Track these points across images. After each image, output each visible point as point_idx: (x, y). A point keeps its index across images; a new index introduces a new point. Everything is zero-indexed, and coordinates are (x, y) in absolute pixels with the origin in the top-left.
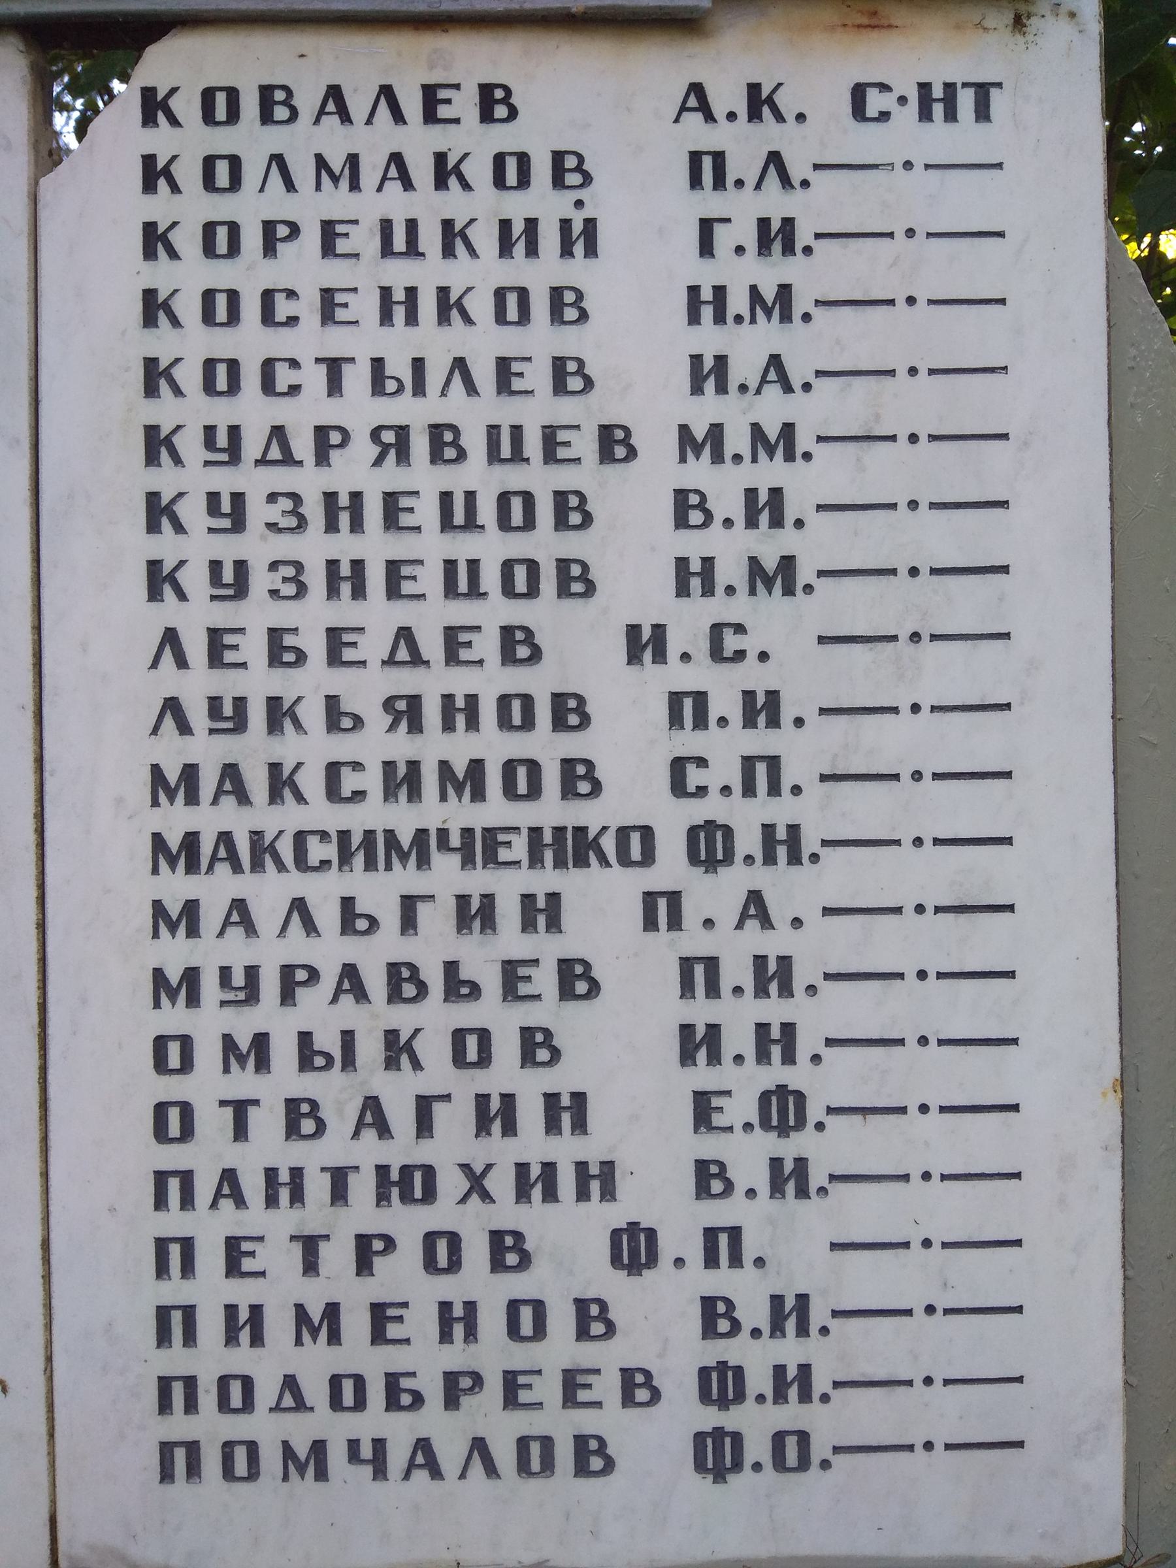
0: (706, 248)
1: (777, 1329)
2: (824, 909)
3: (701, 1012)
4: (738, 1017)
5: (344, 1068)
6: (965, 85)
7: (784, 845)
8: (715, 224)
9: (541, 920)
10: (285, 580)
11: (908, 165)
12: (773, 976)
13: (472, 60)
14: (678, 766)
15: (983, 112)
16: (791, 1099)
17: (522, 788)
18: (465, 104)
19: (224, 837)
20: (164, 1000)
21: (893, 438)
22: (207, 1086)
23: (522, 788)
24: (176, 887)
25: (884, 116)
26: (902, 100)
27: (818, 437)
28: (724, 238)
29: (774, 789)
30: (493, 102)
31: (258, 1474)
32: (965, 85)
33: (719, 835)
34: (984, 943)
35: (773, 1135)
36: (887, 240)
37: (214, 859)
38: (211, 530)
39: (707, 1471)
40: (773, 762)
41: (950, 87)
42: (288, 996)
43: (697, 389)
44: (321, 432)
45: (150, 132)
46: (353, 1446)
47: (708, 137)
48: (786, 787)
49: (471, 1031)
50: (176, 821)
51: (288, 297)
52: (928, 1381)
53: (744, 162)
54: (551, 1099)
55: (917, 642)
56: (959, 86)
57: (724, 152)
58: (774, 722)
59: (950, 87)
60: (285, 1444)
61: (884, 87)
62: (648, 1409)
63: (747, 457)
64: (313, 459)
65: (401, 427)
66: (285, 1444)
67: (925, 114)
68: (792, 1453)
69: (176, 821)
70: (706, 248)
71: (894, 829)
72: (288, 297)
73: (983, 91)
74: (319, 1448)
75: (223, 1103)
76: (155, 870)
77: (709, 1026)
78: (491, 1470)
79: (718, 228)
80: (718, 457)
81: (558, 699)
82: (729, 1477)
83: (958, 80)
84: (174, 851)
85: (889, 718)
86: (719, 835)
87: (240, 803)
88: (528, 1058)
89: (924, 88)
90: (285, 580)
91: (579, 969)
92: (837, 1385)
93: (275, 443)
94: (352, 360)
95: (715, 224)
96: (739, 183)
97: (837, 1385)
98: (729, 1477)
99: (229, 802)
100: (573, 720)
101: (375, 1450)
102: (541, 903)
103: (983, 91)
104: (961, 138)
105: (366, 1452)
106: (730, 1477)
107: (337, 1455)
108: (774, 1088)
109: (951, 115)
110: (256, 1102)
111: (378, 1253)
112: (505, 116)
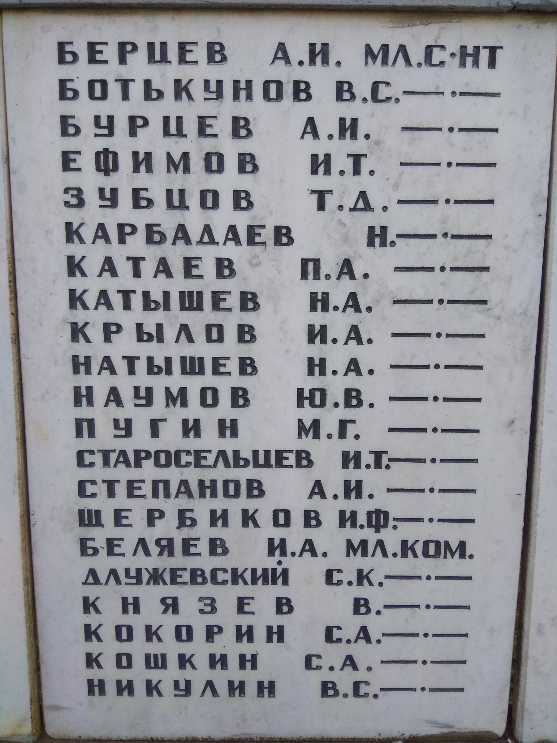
1: (312, 62)
2: (384, 605)
5: (158, 341)
6: (484, 47)
10: (73, 196)
13: (199, 30)
15: (492, 64)
17: (209, 401)
18: (200, 53)
23: (209, 401)
25: (442, 63)
30: (216, 53)
32: (484, 47)
33: (110, 156)
41: (477, 48)
44: (121, 227)
45: (70, 245)
47: (321, 147)
51: (187, 454)
59: (477, 48)
60: (168, 154)
61: (442, 47)
63: (341, 309)
64: (198, 495)
65: (174, 597)
66: (168, 154)
67: (463, 64)
71: (411, 360)
72: (187, 454)
73: (493, 50)
75: (313, 192)
86: (110, 156)
87: (107, 243)
90: (73, 196)
96: (335, 372)
103: (493, 50)
104: (479, 77)
106: (382, 530)
109: (476, 63)
111: (129, 52)
112: (227, 275)
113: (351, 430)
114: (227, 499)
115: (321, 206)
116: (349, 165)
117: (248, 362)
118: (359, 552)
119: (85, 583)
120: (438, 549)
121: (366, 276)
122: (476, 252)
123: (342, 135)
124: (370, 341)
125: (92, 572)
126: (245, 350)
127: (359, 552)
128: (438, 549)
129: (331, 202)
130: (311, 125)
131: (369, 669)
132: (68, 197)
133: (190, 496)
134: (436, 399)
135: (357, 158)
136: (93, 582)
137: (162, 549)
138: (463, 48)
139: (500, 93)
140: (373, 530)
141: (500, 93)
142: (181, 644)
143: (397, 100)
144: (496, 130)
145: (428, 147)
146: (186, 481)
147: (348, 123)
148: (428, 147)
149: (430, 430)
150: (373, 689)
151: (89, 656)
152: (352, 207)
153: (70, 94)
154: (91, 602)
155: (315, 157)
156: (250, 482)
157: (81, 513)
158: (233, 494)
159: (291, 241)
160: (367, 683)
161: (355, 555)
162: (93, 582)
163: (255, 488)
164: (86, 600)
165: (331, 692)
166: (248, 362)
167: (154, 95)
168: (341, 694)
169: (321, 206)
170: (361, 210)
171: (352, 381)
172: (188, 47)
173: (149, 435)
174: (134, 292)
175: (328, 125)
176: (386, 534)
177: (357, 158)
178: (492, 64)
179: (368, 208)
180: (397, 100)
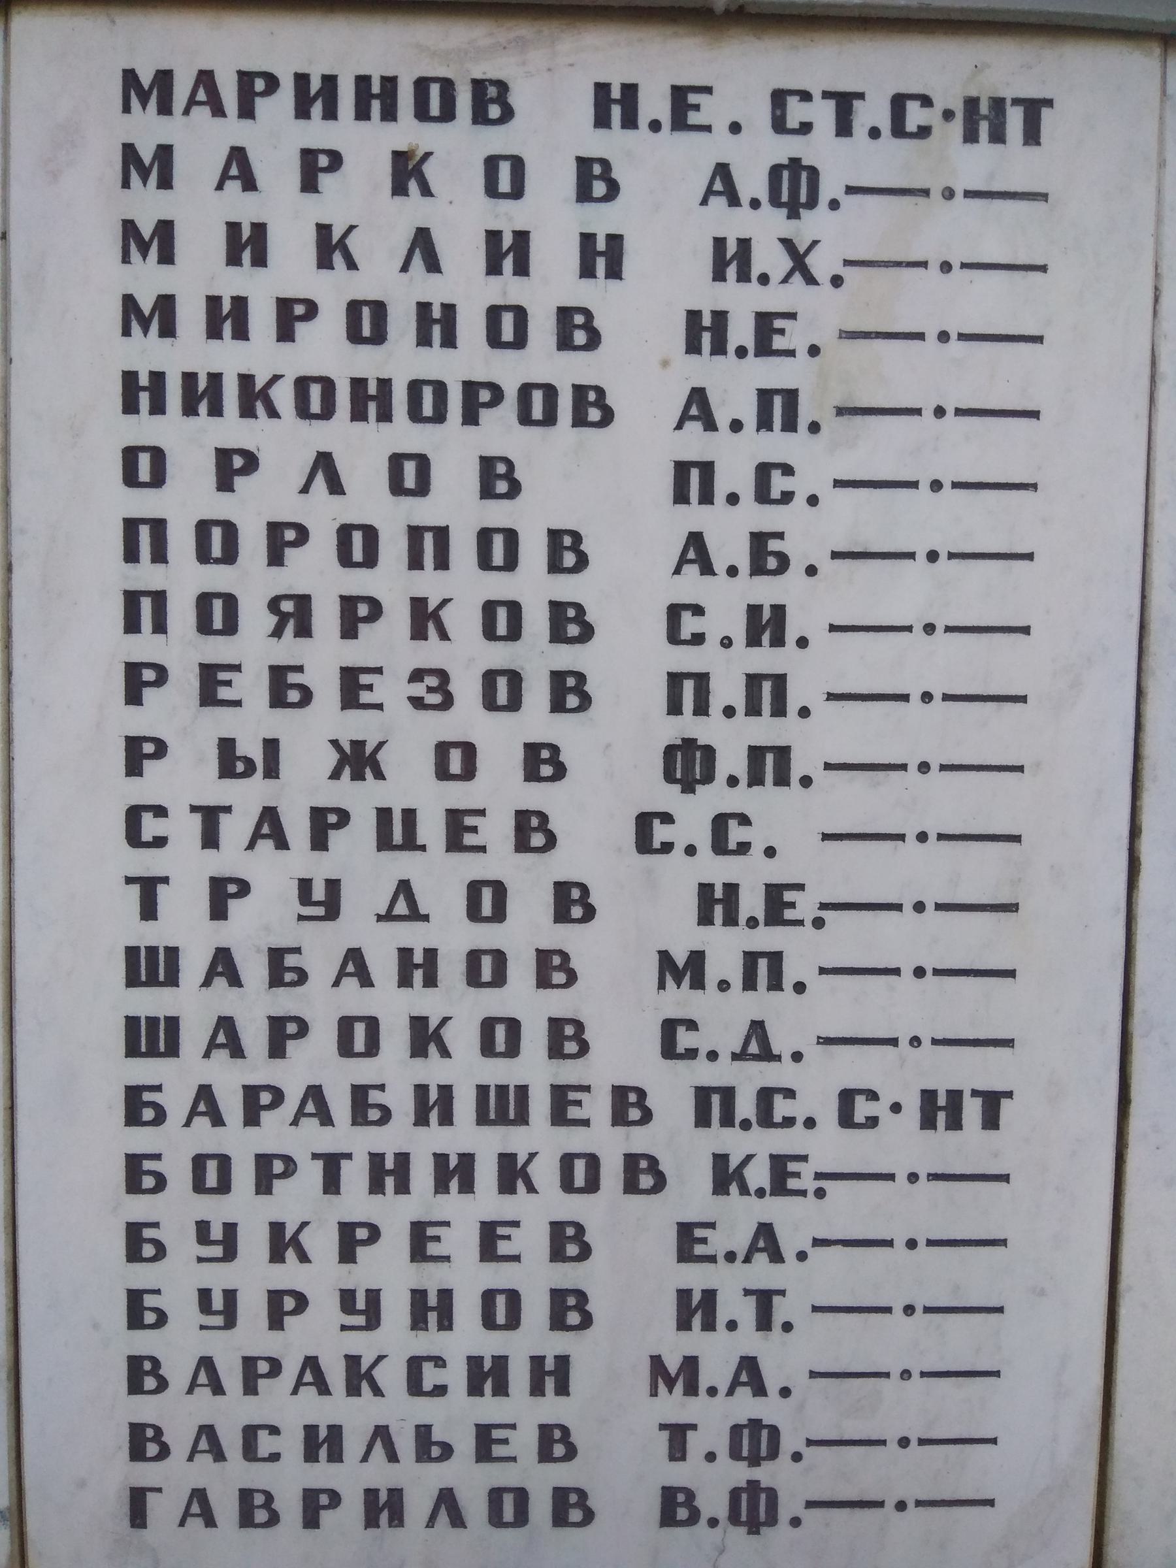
0: (678, 1452)
7: (770, 765)
10: (430, 690)
14: (669, 1027)
15: (1032, 135)
16: (804, 175)
19: (204, 78)
20: (136, 328)
21: (924, 264)
22: (175, 1211)
24: (148, 130)
26: (948, 115)
27: (811, 1372)
28: (696, 1444)
34: (972, 1275)
35: (743, 1530)
36: (921, 270)
37: (192, 102)
39: (744, 1459)
40: (780, 681)
41: (998, 104)
42: (264, 1185)
43: (719, 275)
47: (734, 224)
49: (455, 745)
50: (148, 353)
53: (736, 474)
55: (924, 773)
56: (1009, 102)
58: (778, 641)
67: (971, 136)
69: (148, 353)
70: (678, 1452)
73: (1034, 108)
76: (126, 184)
78: (457, 1520)
80: (692, 1389)
82: (763, 1530)
83: (1009, 94)
84: (146, 86)
89: (929, 1096)
90: (430, 690)
91: (571, 682)
92: (851, 190)
94: (349, 1156)
97: (851, 190)
99: (205, 1460)
103: (1034, 108)
104: (1012, 164)
108: (786, 162)
109: (955, 1123)
110: (228, 809)
116: (746, 1312)
118: (679, 1387)
122: (972, 1275)
126: (567, 588)
127: (679, 1387)
128: (981, 119)
130: (723, 183)
131: (797, 1057)
132: (419, 690)
135: (765, 1300)
137: (283, 618)
138: (971, 104)
139: (1012, 1040)
140: (784, 211)
141: (1012, 1040)
142: (264, 69)
144: (1011, 974)
149: (915, 697)
152: (738, 1051)
153: (294, 696)
155: (719, 243)
157: (132, 1023)
160: (790, 1093)
161: (670, 1392)
163: (500, 477)
165: (559, 978)
167: (435, 1451)
171: (766, 591)
172: (497, 1434)
174: (349, 1156)
176: (813, 224)
177: (765, 1300)
178: (1032, 135)
179: (767, 1055)
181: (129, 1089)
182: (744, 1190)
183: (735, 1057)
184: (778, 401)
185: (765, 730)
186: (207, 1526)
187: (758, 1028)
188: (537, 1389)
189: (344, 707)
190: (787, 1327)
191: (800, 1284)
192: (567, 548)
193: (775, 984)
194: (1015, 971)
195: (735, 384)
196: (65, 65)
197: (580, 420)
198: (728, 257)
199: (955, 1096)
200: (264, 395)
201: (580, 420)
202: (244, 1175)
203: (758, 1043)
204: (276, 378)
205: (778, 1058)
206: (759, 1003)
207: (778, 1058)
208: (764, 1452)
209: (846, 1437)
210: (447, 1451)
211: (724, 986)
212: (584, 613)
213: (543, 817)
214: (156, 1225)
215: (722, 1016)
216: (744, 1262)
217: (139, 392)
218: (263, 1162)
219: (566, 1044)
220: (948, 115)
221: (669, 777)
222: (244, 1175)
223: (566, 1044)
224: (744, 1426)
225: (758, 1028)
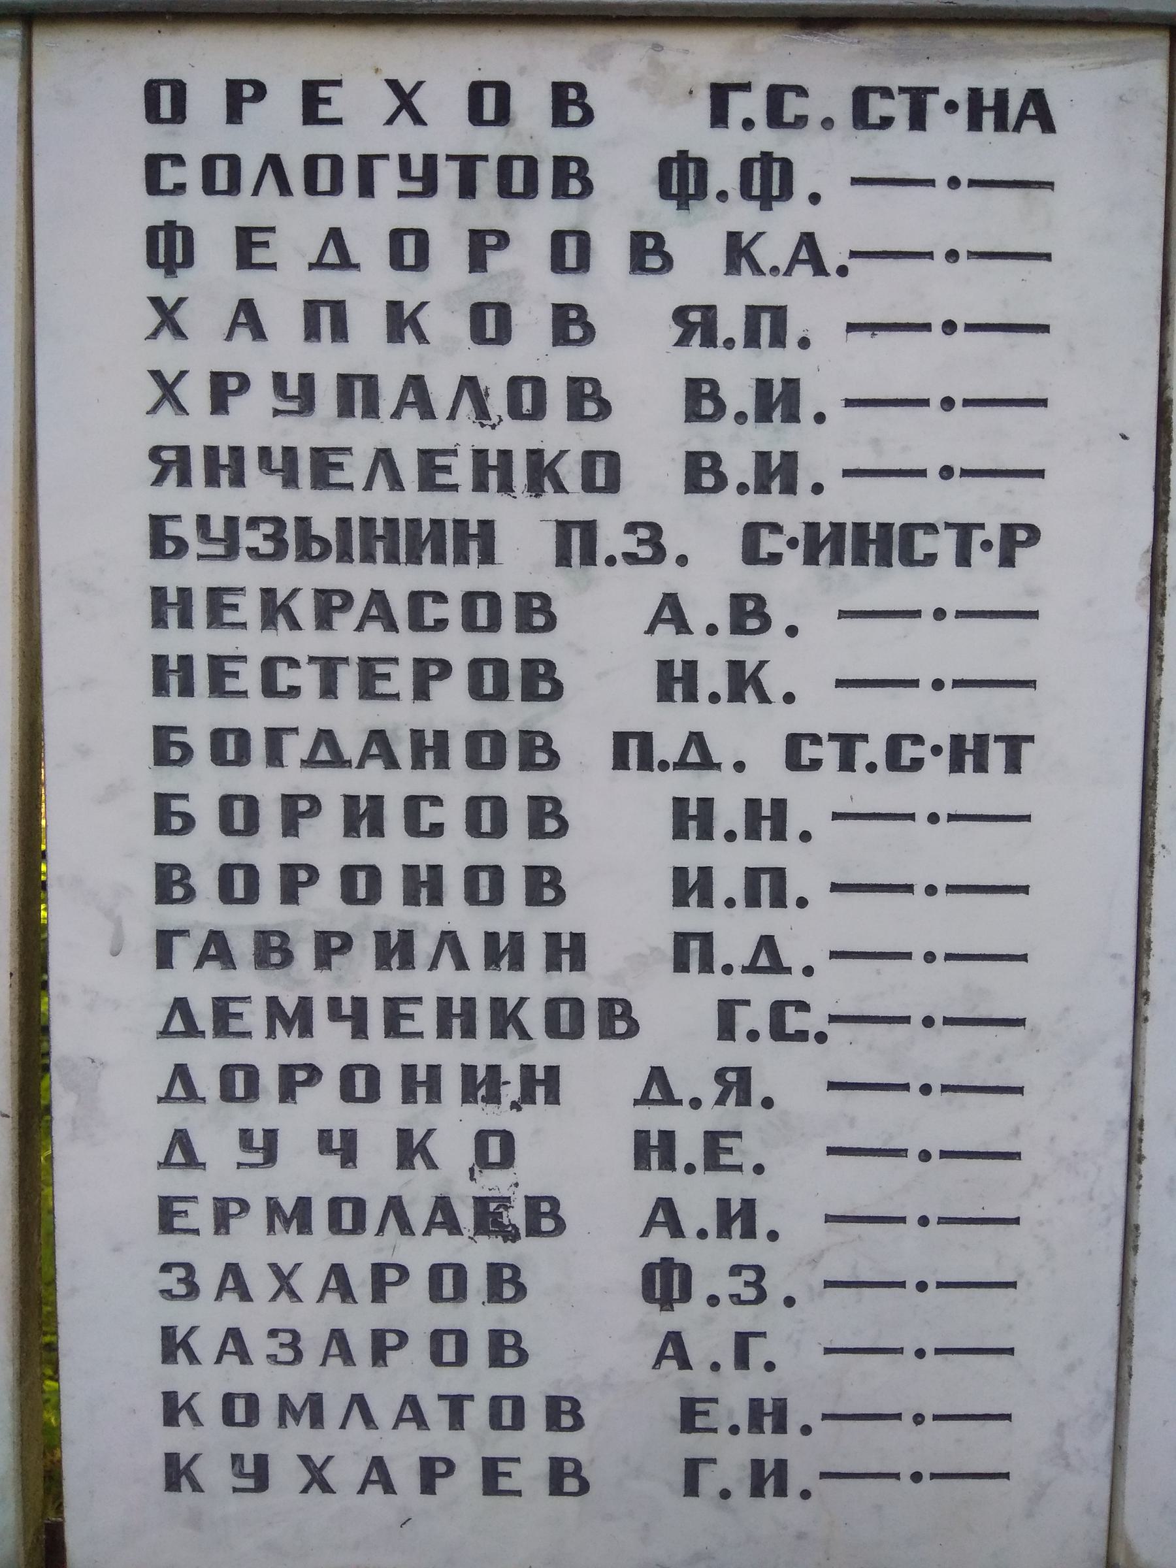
3: (692, 853)
4: (729, 863)
5: (340, 559)
8: (750, 1339)
9: (566, 959)
11: (920, 1353)
12: (768, 1415)
15: (1013, 765)
28: (744, 1019)
29: (778, 339)
31: (256, 1097)
38: (235, 1490)
46: (334, 1004)
48: (791, 900)
52: (920, 1353)
54: (553, 939)
57: (785, 1432)
62: (579, 129)
68: (768, 1478)
73: (1014, 744)
74: (305, 1005)
77: (701, 869)
79: (740, 1011)
81: (607, 1004)
82: (180, 272)
85: (925, 262)
88: (534, 898)
93: (331, 246)
95: (750, 1339)
98: (180, 272)
100: (576, 332)
101: (301, 386)
102: (566, 943)
103: (1014, 744)
104: (988, 789)
105: (347, 1009)
107: (320, 1011)
109: (981, 766)
113: (758, 1352)
114: (470, 634)
115: (692, 1487)
117: (539, 741)
119: (166, 1163)
120: (966, 753)
121: (789, 698)
123: (724, 1230)
124: (804, 343)
125: (181, 1072)
128: (966, 753)
129: (709, 1480)
131: (808, 971)
133: (391, 625)
134: (922, 1286)
136: (183, 1160)
143: (805, 836)
145: (872, 1118)
146: (414, 1397)
147: (737, 1228)
148: (872, 1118)
149: (919, 889)
150: (813, 1022)
151: (171, 1459)
152: (747, 964)
154: (179, 1337)
156: (527, 736)
158: (504, 1402)
159: (633, 1029)
162: (183, 1160)
164: (168, 1333)
166: (539, 741)
168: (731, 412)
169: (692, 1487)
170: (763, 970)
173: (299, 118)
175: (697, 1210)
178: (1013, 765)
179: (777, 967)
180: (821, 1037)
181: (158, 729)
182: (757, 269)
183: (745, 970)
184: (765, 880)
185: (775, 438)
186: (243, 1362)
187: (767, 943)
188: (553, 964)
189: (305, 122)
190: (802, 902)
191: (829, 369)
192: (509, 1347)
193: (778, 901)
194: (1028, 886)
195: (736, 372)
196: (95, 78)
197: (607, 1032)
198: (733, 1213)
199: (981, 740)
200: (286, 608)
201: (607, 1032)
202: (271, 815)
203: (768, 956)
204: (295, 592)
205: (788, 970)
206: (766, 919)
207: (788, 970)
208: (757, 167)
209: (852, 1291)
210: (182, 546)
211: (712, 629)
212: (585, 95)
213: (550, 665)
214: (185, 797)
215: (735, 932)
216: (785, 274)
217: (171, 463)
218: (289, 801)
219: (648, 258)
220: (937, 750)
221: (665, 193)
222: (271, 815)
223: (648, 258)
224: (756, 160)
225: (767, 943)
